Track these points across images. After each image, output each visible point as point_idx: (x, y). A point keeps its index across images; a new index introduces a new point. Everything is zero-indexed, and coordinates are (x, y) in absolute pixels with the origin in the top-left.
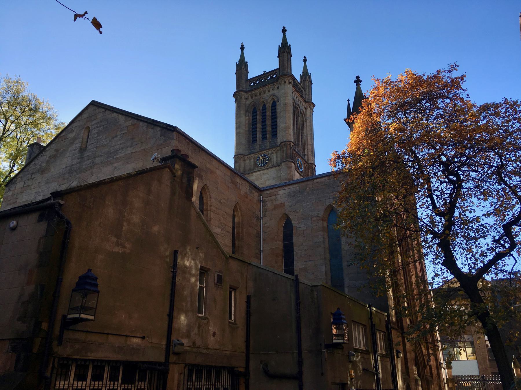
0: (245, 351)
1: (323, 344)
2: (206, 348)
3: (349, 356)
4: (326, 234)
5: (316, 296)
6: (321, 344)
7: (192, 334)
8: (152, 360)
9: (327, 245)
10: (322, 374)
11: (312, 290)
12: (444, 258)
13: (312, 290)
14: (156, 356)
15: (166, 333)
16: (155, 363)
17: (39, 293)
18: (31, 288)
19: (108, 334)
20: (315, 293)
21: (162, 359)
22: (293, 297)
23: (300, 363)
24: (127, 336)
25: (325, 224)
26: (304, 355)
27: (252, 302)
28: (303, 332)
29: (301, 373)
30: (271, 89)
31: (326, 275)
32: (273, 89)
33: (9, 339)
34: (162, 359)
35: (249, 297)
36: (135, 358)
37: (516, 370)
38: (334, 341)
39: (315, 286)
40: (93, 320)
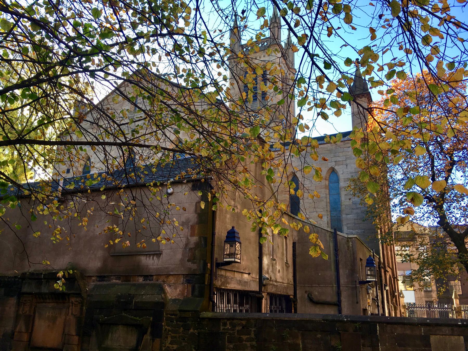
0: (293, 283)
1: (358, 281)
2: (276, 281)
3: (367, 289)
4: (328, 191)
5: (351, 245)
6: (356, 281)
7: (270, 271)
8: (253, 290)
9: (328, 200)
10: (357, 303)
11: (348, 241)
12: (439, 219)
13: (348, 241)
14: (254, 287)
15: (258, 271)
16: (253, 292)
17: (203, 243)
18: (194, 239)
19: (234, 271)
20: (351, 243)
21: (257, 289)
22: (332, 245)
23: (339, 294)
24: (242, 273)
25: (327, 183)
26: (341, 288)
27: (297, 247)
28: (341, 271)
29: (339, 301)
30: (262, 56)
31: (328, 224)
32: (264, 56)
33: (183, 274)
34: (257, 289)
35: (294, 244)
36: (247, 289)
37: (456, 300)
38: (225, 260)
39: (350, 238)
40: (240, 263)
